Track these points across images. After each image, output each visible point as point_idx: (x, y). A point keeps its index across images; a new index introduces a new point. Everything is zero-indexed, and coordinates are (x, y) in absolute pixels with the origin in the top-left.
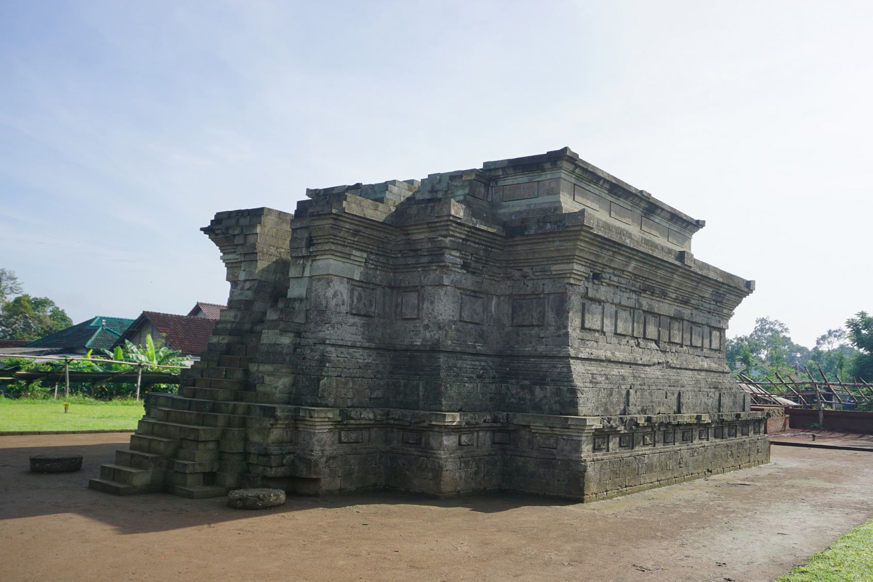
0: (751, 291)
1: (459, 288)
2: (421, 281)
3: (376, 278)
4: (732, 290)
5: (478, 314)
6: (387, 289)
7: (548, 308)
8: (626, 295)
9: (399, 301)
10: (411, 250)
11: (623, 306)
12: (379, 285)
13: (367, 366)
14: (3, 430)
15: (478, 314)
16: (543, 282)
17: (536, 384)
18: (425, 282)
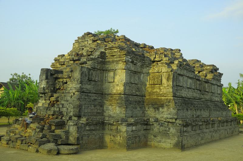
0: (109, 37)
1: (130, 70)
2: (115, 68)
3: (98, 67)
4: (218, 69)
5: (136, 80)
6: (102, 71)
7: (163, 78)
8: (191, 73)
9: (107, 75)
10: (111, 56)
11: (189, 77)
12: (99, 69)
13: (107, 100)
14: (1, 124)
15: (136, 80)
16: (161, 68)
17: (160, 107)
18: (117, 68)
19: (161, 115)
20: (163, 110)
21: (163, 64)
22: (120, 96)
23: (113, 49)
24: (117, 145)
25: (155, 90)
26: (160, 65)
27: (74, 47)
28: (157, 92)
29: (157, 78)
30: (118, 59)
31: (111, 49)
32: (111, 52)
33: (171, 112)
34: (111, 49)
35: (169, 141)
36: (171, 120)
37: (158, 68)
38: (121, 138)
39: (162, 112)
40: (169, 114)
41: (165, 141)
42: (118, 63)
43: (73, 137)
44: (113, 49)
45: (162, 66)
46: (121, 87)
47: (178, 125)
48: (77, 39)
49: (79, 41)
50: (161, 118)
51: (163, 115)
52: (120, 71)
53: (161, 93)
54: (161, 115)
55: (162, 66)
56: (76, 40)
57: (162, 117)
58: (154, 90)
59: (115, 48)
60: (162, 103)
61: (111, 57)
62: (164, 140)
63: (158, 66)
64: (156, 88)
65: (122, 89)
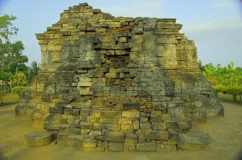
18: (168, 42)
19: (197, 89)
20: (198, 84)
21: (190, 43)
22: (177, 72)
23: (168, 22)
24: (195, 122)
25: (182, 66)
26: (187, 43)
27: (62, 17)
28: (184, 68)
29: (183, 55)
30: (171, 33)
31: (166, 21)
32: (164, 25)
33: (206, 85)
34: (166, 21)
35: (213, 110)
36: (206, 92)
37: (184, 46)
38: (201, 114)
39: (198, 86)
40: (205, 87)
41: (210, 111)
42: (170, 37)
43: (186, 121)
44: (168, 22)
45: (188, 44)
46: (175, 62)
47: (214, 96)
48: (68, 9)
49: (70, 12)
50: (196, 91)
51: (198, 89)
52: (171, 46)
53: (189, 68)
54: (197, 89)
55: (188, 44)
56: (65, 11)
57: (198, 90)
58: (180, 66)
59: (172, 21)
60: (194, 77)
61: (162, 30)
62: (209, 110)
63: (184, 44)
64: (183, 64)
65: (176, 64)
